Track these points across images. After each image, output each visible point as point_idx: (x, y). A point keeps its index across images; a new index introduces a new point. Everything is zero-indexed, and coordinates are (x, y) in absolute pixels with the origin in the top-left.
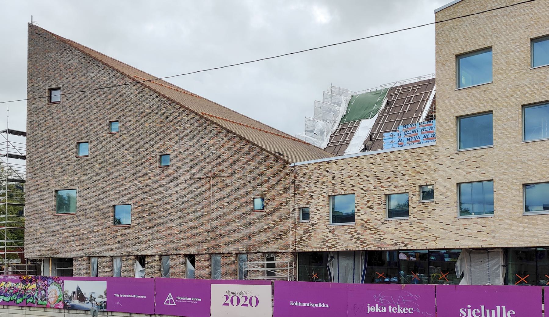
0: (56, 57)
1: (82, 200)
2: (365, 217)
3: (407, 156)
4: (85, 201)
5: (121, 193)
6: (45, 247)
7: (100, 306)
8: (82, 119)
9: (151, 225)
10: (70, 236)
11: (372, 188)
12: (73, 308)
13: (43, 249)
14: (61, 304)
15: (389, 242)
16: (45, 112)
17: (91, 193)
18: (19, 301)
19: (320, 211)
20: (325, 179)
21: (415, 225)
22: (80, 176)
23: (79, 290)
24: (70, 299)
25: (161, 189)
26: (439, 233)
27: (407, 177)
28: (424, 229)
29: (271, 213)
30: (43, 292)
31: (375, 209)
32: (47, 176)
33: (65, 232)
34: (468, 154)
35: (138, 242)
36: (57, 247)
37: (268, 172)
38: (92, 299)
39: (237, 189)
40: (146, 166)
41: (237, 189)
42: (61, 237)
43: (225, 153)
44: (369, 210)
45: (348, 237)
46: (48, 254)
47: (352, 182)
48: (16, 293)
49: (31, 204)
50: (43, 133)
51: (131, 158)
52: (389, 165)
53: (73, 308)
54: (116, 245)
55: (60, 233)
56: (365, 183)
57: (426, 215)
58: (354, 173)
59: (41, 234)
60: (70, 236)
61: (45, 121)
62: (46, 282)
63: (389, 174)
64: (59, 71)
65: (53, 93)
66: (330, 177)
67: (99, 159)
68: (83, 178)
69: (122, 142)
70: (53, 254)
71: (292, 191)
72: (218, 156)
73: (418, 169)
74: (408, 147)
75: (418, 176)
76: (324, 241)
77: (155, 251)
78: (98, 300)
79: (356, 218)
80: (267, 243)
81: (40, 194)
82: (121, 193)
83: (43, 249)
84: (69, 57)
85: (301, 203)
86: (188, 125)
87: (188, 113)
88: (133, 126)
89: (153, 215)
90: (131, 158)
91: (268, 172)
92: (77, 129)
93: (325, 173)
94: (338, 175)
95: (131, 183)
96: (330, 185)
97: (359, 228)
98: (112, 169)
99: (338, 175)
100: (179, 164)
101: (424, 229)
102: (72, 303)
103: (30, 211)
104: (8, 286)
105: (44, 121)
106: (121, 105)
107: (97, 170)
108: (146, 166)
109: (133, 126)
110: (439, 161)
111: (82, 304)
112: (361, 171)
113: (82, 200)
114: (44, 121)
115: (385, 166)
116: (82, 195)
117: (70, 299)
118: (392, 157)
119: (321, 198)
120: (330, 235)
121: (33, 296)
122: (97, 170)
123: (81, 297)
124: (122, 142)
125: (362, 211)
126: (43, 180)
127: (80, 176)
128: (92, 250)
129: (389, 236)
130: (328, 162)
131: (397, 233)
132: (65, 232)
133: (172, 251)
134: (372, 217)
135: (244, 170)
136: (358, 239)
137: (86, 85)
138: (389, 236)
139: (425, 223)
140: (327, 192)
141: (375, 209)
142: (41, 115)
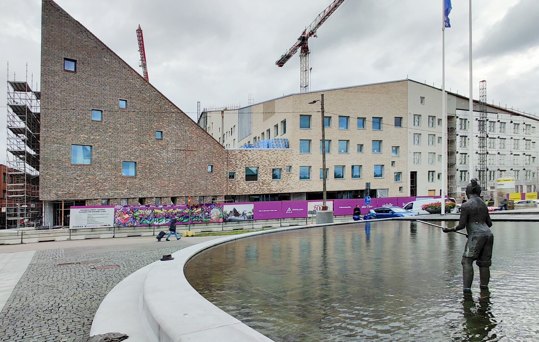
0: (72, 34)
1: (97, 155)
2: (264, 178)
3: (281, 152)
4: (100, 156)
5: (129, 153)
6: (63, 191)
7: (249, 218)
8: (97, 92)
9: (150, 177)
10: (87, 182)
11: (267, 165)
12: (230, 221)
13: (60, 193)
14: (221, 219)
15: (274, 190)
16: (61, 77)
17: (105, 150)
18: (185, 221)
19: (241, 175)
20: (244, 159)
21: (285, 183)
22: (96, 136)
23: (235, 210)
24: (228, 215)
25: (157, 153)
26: (293, 186)
27: (281, 162)
28: (288, 184)
29: (216, 174)
30: (207, 213)
31: (268, 175)
32: (63, 132)
33: (82, 179)
34: (304, 155)
35: (142, 188)
36: (74, 191)
37: (215, 151)
38: (244, 214)
39: (201, 160)
40: (147, 137)
41: (201, 160)
42: (78, 183)
43: (195, 136)
44: (266, 175)
45: (256, 188)
46: (66, 197)
47: (258, 162)
48: (183, 216)
49: (47, 153)
50: (59, 94)
51: (137, 129)
52: (274, 156)
53: (230, 221)
54: (126, 191)
55: (77, 180)
56: (264, 163)
57: (289, 179)
58: (259, 157)
59: (58, 180)
60: (87, 182)
61: (61, 84)
62: (209, 207)
63: (274, 160)
64: (75, 47)
65: (73, 63)
66: (247, 158)
67: (111, 125)
68: (98, 138)
69: (130, 117)
70: (70, 197)
71: (225, 163)
72: (191, 138)
73: (286, 159)
74: (282, 149)
75: (286, 162)
76: (243, 190)
77: (153, 195)
78: (248, 215)
79: (259, 178)
80: (214, 191)
81: (56, 145)
82: (129, 153)
83: (60, 193)
84: (85, 38)
85: (231, 170)
86: (174, 115)
87: (174, 107)
88: (138, 107)
89: (152, 171)
90: (137, 129)
91: (215, 151)
92: (93, 99)
93: (244, 156)
94: (251, 158)
95: (136, 147)
96: (247, 162)
97: (261, 184)
98: (122, 135)
99: (251, 157)
100: (168, 139)
101: (288, 184)
102: (230, 218)
103: (46, 160)
104: (176, 211)
105: (60, 84)
106: (128, 90)
107: (110, 134)
108: (147, 137)
109: (138, 107)
110: (294, 156)
111: (237, 218)
112: (262, 157)
113: (97, 155)
114: (60, 84)
115: (273, 156)
116: (98, 151)
117: (228, 215)
118: (275, 152)
119: (242, 168)
120: (247, 187)
121: (198, 217)
122: (110, 134)
123: (236, 213)
124: (130, 117)
125: (262, 176)
126: (59, 134)
127: (96, 136)
128: (106, 194)
129: (274, 187)
130: (246, 150)
131: (277, 186)
132: (82, 179)
133: (164, 195)
134: (267, 179)
135: (204, 148)
136: (260, 189)
137: (101, 66)
138: (274, 187)
139: (289, 182)
140: (245, 165)
141: (268, 175)
142: (57, 78)
